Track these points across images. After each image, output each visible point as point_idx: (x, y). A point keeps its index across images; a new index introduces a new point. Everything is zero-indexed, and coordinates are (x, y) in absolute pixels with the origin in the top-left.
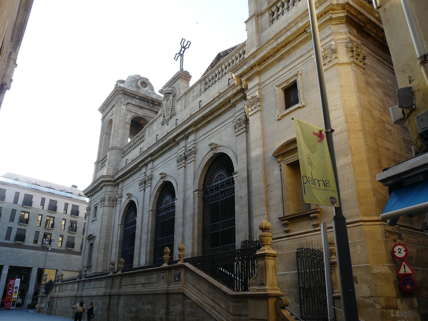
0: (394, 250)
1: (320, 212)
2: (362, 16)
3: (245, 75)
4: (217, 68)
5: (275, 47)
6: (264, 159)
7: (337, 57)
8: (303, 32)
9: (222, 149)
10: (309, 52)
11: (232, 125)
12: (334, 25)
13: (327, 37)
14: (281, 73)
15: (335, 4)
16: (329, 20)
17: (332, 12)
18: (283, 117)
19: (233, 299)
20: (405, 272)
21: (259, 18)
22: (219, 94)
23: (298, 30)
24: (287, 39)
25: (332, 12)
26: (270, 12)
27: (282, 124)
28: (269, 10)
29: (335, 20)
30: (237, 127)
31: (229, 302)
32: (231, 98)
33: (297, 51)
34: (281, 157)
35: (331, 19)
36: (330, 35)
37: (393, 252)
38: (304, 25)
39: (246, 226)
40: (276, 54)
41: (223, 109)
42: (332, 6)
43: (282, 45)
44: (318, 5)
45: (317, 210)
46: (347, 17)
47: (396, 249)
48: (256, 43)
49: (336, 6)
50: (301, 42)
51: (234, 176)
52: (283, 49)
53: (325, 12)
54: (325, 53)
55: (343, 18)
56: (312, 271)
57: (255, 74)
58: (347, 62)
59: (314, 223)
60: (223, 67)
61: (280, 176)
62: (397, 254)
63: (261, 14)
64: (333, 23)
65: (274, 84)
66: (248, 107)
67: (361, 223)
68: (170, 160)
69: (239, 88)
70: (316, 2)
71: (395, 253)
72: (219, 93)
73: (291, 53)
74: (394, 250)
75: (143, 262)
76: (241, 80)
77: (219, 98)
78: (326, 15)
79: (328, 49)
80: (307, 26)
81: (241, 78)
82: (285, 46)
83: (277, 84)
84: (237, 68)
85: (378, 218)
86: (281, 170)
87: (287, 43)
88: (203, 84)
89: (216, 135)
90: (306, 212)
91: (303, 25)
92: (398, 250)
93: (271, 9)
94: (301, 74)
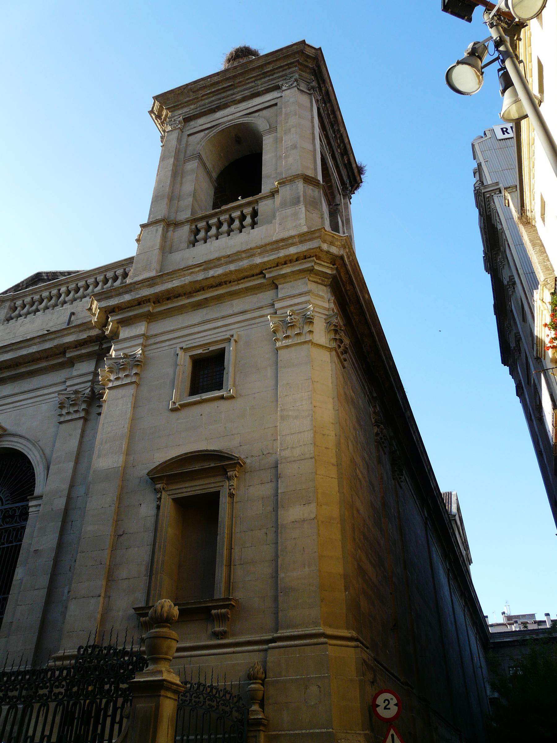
0: (377, 703)
1: (235, 606)
2: (351, 287)
3: (122, 311)
4: (48, 288)
5: (200, 280)
6: (124, 479)
7: (313, 332)
8: (257, 275)
9: (17, 442)
11: (55, 399)
12: (312, 281)
13: (300, 295)
14: (196, 329)
15: (325, 250)
16: (308, 270)
17: (315, 260)
18: (183, 406)
21: (170, 229)
22: (46, 332)
23: (252, 267)
24: (225, 274)
25: (315, 260)
26: (194, 227)
27: (178, 419)
28: (191, 223)
30: (66, 405)
32: (68, 348)
33: (235, 302)
34: (164, 482)
35: (311, 271)
36: (306, 293)
39: (35, 619)
40: (194, 294)
41: (44, 364)
42: (319, 250)
44: (297, 241)
45: (230, 603)
46: (334, 277)
47: (380, 700)
48: (155, 265)
49: (325, 253)
51: (31, 503)
52: (211, 289)
53: (305, 256)
54: (293, 318)
56: (202, 740)
58: (325, 345)
59: (217, 629)
60: (63, 289)
61: (153, 519)
62: (380, 711)
63: (175, 224)
64: (311, 279)
65: (177, 343)
66: (111, 372)
67: (323, 640)
68: (174, 339)
69: (95, 332)
70: (296, 236)
71: (378, 709)
72: (47, 331)
74: (377, 703)
75: (110, 714)
76: (108, 318)
77: (43, 339)
78: (304, 261)
79: (298, 314)
80: (267, 267)
81: (111, 314)
82: (217, 286)
83: (184, 345)
84: (110, 294)
85: (350, 633)
86: (158, 507)
87: (222, 282)
88: (7, 308)
89: (8, 410)
90: (205, 602)
91: (262, 261)
92: (384, 702)
93: (196, 224)
94: (236, 341)
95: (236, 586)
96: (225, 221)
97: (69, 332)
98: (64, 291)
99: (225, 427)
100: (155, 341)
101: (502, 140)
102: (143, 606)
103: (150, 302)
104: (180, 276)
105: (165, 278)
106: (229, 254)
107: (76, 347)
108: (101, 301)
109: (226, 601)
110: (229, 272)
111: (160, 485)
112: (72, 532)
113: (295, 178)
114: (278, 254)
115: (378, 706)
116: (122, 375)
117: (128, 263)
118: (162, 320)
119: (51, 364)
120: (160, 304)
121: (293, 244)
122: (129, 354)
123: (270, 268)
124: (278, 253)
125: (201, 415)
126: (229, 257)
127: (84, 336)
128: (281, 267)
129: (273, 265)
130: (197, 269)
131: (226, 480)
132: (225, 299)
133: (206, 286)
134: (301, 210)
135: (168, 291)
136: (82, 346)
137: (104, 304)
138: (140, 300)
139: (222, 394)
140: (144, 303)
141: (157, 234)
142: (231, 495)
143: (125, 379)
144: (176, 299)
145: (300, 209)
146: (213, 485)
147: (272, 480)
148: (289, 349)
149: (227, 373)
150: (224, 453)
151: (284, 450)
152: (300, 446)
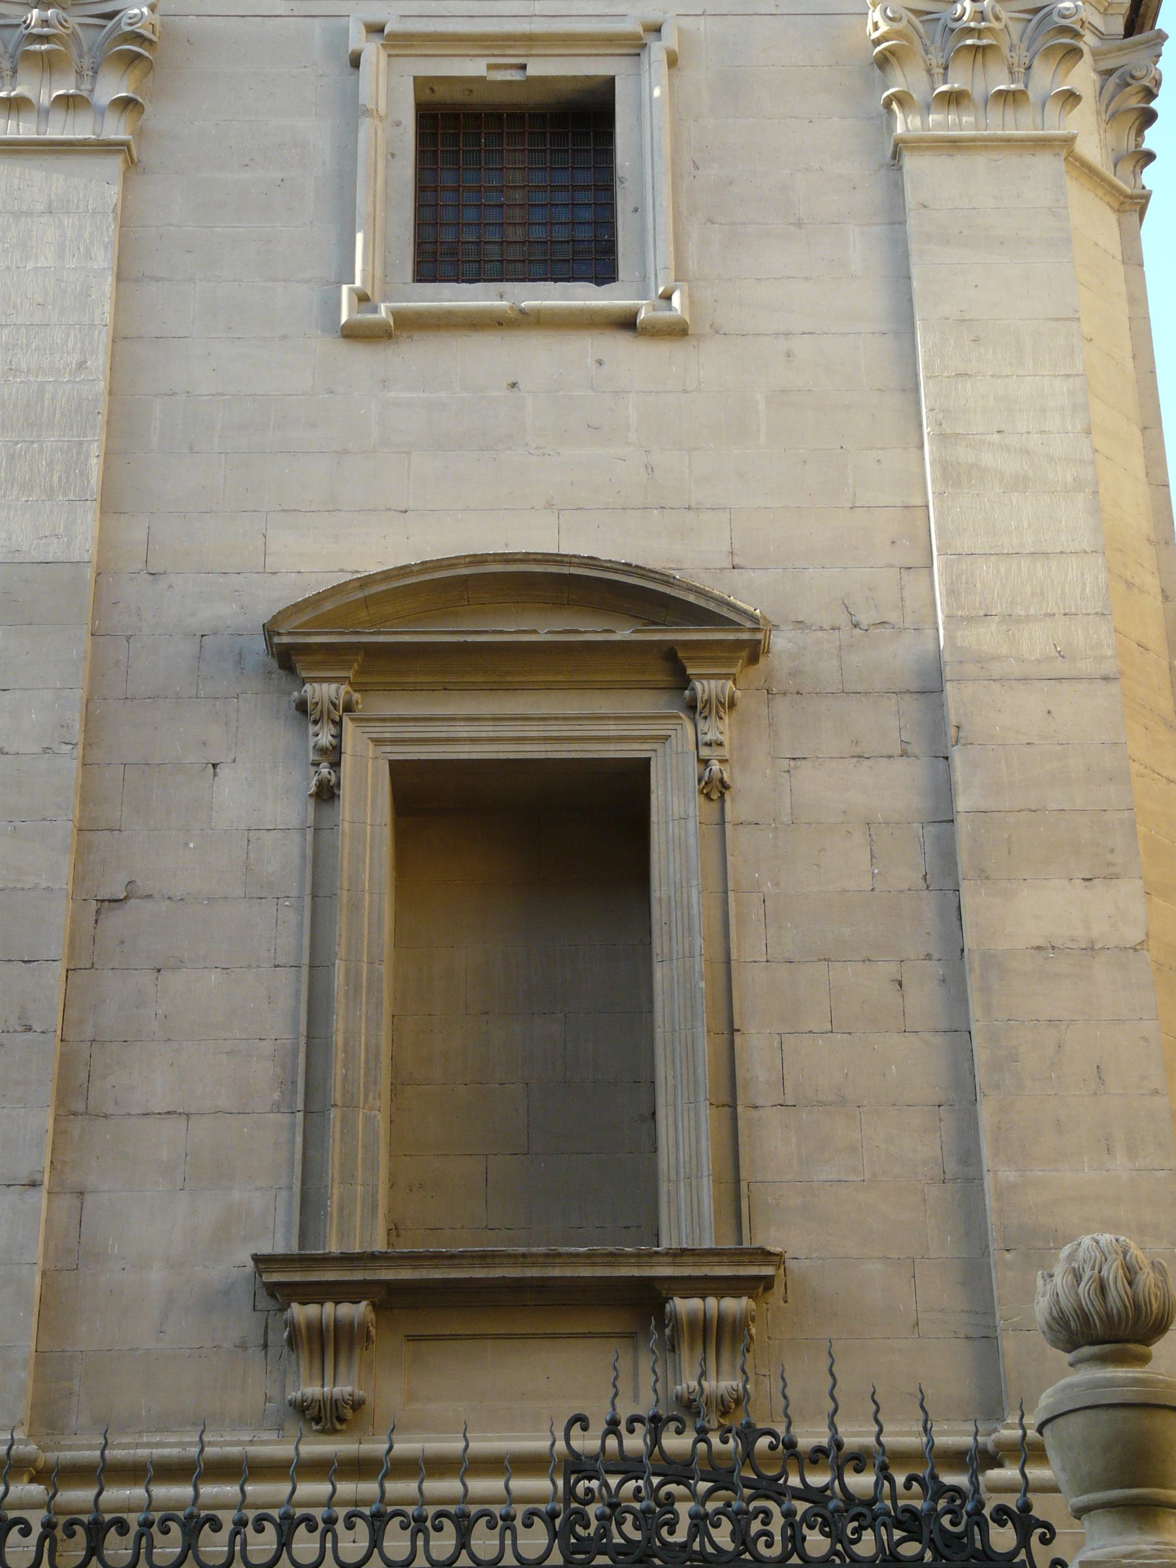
27: (384, 384)
34: (350, 674)
94: (673, 61)
99: (650, 469)
102: (280, 1249)
109: (752, 1263)
111: (334, 686)
116: (44, 92)
131: (681, 715)
146: (611, 729)
147: (910, 749)
148: (959, 162)
149: (636, 210)
150: (681, 587)
151: (970, 619)
152: (1046, 615)
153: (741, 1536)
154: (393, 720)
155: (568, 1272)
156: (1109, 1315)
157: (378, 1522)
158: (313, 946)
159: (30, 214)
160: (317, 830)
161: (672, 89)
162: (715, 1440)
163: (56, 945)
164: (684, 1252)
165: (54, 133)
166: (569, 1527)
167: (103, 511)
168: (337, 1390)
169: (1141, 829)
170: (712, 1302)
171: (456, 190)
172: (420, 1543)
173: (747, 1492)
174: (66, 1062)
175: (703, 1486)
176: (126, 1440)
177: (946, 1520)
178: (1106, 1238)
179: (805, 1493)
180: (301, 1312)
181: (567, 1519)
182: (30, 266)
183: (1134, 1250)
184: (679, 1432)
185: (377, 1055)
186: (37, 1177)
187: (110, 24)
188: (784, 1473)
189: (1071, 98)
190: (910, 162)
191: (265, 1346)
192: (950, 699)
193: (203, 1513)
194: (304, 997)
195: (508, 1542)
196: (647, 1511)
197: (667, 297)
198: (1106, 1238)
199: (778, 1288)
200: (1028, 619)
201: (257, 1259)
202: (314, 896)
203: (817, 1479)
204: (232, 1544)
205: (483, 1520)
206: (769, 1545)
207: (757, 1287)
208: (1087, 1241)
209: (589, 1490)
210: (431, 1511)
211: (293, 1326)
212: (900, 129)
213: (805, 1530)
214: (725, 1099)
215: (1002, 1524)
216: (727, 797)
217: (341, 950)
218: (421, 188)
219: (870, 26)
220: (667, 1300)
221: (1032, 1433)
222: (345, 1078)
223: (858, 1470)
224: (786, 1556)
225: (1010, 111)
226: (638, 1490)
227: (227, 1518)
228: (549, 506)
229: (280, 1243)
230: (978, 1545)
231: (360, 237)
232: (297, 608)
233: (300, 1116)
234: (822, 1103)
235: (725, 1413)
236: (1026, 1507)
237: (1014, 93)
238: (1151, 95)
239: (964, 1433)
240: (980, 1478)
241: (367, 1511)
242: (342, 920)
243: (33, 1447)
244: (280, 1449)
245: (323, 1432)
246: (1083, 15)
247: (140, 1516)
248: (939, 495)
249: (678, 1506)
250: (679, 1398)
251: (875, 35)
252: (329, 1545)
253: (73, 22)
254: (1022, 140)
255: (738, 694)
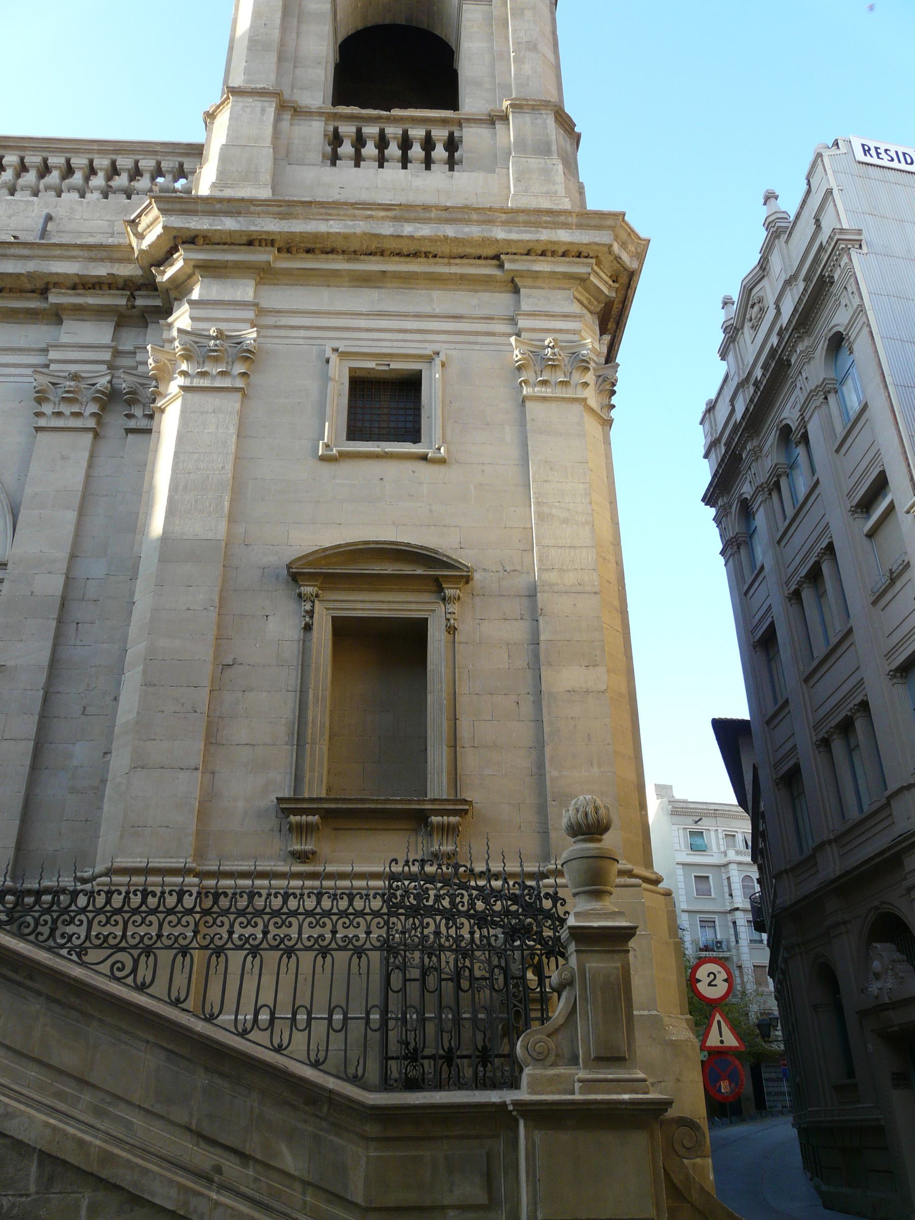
3: (210, 247)
5: (385, 236)
8: (486, 258)
10: (487, 321)
13: (565, 316)
14: (363, 323)
18: (344, 456)
19: (372, 1129)
20: (722, 1042)
22: (12, 240)
24: (433, 240)
26: (331, 128)
27: (334, 477)
29: (586, 290)
31: (337, 1140)
32: (56, 285)
33: (436, 294)
34: (318, 584)
35: (582, 280)
36: (575, 317)
37: (693, 981)
38: (508, 242)
40: (363, 257)
43: (406, 247)
47: (702, 973)
49: (611, 258)
50: (464, 279)
52: (397, 258)
55: (602, 298)
57: (249, 268)
62: (702, 987)
63: (295, 111)
71: (698, 985)
73: (414, 286)
78: (578, 259)
79: (561, 348)
80: (510, 251)
81: (186, 246)
82: (408, 255)
83: (336, 344)
84: (192, 207)
92: (708, 976)
94: (443, 365)
95: (468, 782)
96: (395, 138)
97: (66, 253)
98: (15, 163)
100: (276, 322)
101: (862, 163)
102: (287, 796)
103: (272, 245)
104: (345, 215)
105: (315, 210)
106: (448, 204)
107: (74, 288)
108: (170, 213)
109: (460, 804)
110: (442, 237)
112: (78, 643)
113: (543, 105)
114: (537, 235)
115: (699, 981)
116: (215, 370)
117: (166, 152)
118: (287, 287)
119: (9, 306)
120: (289, 255)
121: (566, 226)
122: (227, 333)
123: (515, 254)
124: (537, 232)
125: (382, 479)
126: (446, 210)
127: (101, 270)
128: (534, 258)
129: (519, 251)
130: (382, 214)
132: (418, 284)
133: (389, 249)
134: (555, 167)
135: (316, 236)
136: (89, 288)
137: (178, 222)
138: (254, 237)
139: (423, 452)
140: (260, 245)
141: (265, 118)
142: (452, 630)
143: (218, 379)
144: (324, 256)
145: (554, 164)
146: (414, 607)
147: (524, 617)
148: (547, 405)
153: (453, 903)
154: (334, 601)
155: (393, 806)
156: (588, 825)
157: (319, 896)
158: (301, 683)
159: (207, 413)
160: (304, 641)
161: (443, 375)
162: (444, 868)
163: (207, 682)
164: (435, 800)
165: (217, 385)
166: (390, 899)
167: (229, 521)
168: (306, 847)
169: (606, 648)
170: (445, 818)
171: (363, 408)
172: (335, 903)
173: (455, 887)
174: (209, 724)
175: (439, 885)
176: (229, 863)
177: (527, 898)
178: (588, 797)
179: (477, 888)
180: (293, 819)
181: (389, 896)
182: (206, 431)
183: (598, 802)
184: (431, 865)
185: (324, 726)
186: (198, 767)
187: (239, 346)
188: (469, 881)
189: (586, 384)
190: (528, 404)
191: (280, 831)
192: (539, 601)
193: (255, 891)
194: (298, 702)
195: (367, 904)
196: (419, 893)
197: (439, 449)
198: (588, 797)
199: (470, 814)
200: (568, 570)
201: (278, 799)
202: (302, 665)
203: (481, 883)
204: (266, 902)
205: (359, 896)
206: (463, 906)
207: (463, 813)
208: (581, 798)
209: (397, 886)
210: (339, 892)
211: (290, 823)
212: (525, 392)
213: (476, 901)
214: (453, 744)
215: (547, 899)
216: (456, 633)
217: (312, 686)
218: (350, 407)
219: (515, 356)
220: (429, 817)
221: (559, 867)
222: (312, 734)
223: (496, 880)
224: (469, 910)
225: (564, 388)
226: (416, 886)
227: (264, 892)
228: (394, 523)
229: (287, 793)
230: (538, 906)
231: (327, 424)
232: (299, 559)
233: (295, 746)
234: (488, 746)
235: (449, 858)
236: (556, 893)
237: (566, 381)
238: (614, 385)
239: (535, 867)
240: (540, 883)
241: (315, 891)
242: (312, 675)
243: (194, 865)
244: (283, 868)
245: (301, 862)
246: (590, 356)
247: (232, 891)
248: (536, 524)
249: (430, 892)
250: (432, 853)
251: (516, 359)
252: (301, 903)
253: (226, 345)
254: (569, 398)
255: (461, 595)
